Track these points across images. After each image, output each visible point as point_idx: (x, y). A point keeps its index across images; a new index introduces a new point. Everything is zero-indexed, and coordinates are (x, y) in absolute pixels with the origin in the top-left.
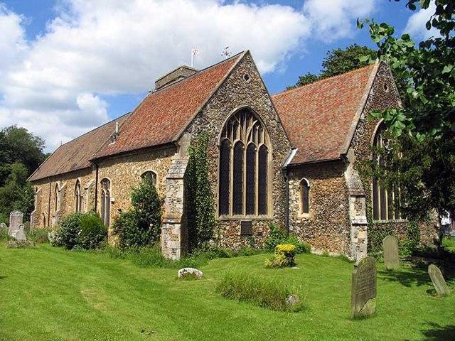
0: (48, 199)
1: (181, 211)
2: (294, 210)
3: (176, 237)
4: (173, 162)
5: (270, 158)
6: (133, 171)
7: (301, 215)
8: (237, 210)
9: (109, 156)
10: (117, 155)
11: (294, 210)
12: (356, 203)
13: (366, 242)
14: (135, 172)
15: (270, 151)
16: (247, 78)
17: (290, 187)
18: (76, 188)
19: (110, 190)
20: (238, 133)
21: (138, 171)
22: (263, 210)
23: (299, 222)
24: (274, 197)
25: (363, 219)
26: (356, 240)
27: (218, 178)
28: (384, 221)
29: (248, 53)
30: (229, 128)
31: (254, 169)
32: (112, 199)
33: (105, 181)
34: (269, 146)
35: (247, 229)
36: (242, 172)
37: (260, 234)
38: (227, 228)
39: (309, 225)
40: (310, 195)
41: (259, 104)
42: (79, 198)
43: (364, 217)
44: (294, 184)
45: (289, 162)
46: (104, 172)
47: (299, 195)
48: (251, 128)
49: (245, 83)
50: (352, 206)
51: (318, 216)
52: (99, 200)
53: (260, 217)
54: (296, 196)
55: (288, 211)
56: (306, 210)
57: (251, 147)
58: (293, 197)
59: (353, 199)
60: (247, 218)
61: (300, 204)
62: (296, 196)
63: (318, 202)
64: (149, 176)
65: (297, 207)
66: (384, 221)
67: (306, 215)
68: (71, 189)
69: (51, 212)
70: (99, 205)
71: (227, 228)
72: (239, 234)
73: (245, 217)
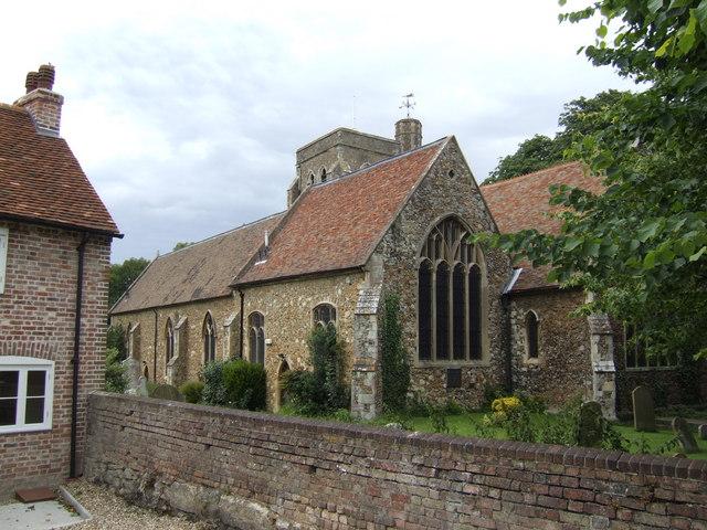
0: (153, 340)
1: (375, 356)
2: (518, 353)
3: (370, 389)
4: (361, 292)
5: (484, 282)
6: (305, 300)
7: (527, 360)
8: (443, 355)
9: (326, 271)
10: (348, 269)
11: (518, 353)
12: (600, 344)
13: (613, 396)
14: (304, 304)
15: (484, 272)
16: (452, 174)
17: (513, 321)
18: (205, 324)
19: (264, 329)
20: (442, 251)
21: (308, 302)
22: (476, 353)
23: (524, 369)
24: (490, 336)
25: (610, 366)
26: (601, 394)
27: (417, 312)
28: (643, 369)
29: (453, 139)
30: (431, 247)
31: (446, 296)
32: (268, 341)
33: (257, 319)
34: (483, 266)
35: (454, 378)
36: (447, 303)
37: (472, 386)
38: (430, 377)
39: (539, 373)
40: (541, 332)
41: (468, 209)
42: (210, 340)
43: (611, 363)
44: (518, 314)
45: (510, 288)
46: (254, 302)
47: (524, 332)
48: (458, 243)
49: (449, 182)
50: (594, 349)
51: (550, 362)
52: (246, 341)
53: (472, 363)
54: (521, 338)
55: (509, 355)
56: (534, 353)
57: (459, 269)
58: (517, 336)
59: (597, 338)
60: (455, 364)
61: (526, 345)
62: (521, 338)
63: (549, 342)
64: (324, 312)
65: (522, 350)
66: (643, 369)
67: (535, 361)
68: (196, 327)
69: (158, 359)
70: (246, 350)
71: (430, 377)
72: (445, 385)
73: (455, 364)
